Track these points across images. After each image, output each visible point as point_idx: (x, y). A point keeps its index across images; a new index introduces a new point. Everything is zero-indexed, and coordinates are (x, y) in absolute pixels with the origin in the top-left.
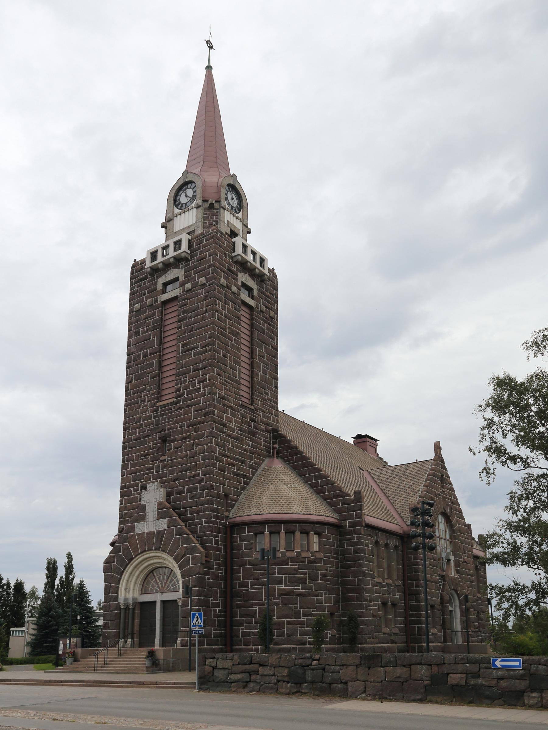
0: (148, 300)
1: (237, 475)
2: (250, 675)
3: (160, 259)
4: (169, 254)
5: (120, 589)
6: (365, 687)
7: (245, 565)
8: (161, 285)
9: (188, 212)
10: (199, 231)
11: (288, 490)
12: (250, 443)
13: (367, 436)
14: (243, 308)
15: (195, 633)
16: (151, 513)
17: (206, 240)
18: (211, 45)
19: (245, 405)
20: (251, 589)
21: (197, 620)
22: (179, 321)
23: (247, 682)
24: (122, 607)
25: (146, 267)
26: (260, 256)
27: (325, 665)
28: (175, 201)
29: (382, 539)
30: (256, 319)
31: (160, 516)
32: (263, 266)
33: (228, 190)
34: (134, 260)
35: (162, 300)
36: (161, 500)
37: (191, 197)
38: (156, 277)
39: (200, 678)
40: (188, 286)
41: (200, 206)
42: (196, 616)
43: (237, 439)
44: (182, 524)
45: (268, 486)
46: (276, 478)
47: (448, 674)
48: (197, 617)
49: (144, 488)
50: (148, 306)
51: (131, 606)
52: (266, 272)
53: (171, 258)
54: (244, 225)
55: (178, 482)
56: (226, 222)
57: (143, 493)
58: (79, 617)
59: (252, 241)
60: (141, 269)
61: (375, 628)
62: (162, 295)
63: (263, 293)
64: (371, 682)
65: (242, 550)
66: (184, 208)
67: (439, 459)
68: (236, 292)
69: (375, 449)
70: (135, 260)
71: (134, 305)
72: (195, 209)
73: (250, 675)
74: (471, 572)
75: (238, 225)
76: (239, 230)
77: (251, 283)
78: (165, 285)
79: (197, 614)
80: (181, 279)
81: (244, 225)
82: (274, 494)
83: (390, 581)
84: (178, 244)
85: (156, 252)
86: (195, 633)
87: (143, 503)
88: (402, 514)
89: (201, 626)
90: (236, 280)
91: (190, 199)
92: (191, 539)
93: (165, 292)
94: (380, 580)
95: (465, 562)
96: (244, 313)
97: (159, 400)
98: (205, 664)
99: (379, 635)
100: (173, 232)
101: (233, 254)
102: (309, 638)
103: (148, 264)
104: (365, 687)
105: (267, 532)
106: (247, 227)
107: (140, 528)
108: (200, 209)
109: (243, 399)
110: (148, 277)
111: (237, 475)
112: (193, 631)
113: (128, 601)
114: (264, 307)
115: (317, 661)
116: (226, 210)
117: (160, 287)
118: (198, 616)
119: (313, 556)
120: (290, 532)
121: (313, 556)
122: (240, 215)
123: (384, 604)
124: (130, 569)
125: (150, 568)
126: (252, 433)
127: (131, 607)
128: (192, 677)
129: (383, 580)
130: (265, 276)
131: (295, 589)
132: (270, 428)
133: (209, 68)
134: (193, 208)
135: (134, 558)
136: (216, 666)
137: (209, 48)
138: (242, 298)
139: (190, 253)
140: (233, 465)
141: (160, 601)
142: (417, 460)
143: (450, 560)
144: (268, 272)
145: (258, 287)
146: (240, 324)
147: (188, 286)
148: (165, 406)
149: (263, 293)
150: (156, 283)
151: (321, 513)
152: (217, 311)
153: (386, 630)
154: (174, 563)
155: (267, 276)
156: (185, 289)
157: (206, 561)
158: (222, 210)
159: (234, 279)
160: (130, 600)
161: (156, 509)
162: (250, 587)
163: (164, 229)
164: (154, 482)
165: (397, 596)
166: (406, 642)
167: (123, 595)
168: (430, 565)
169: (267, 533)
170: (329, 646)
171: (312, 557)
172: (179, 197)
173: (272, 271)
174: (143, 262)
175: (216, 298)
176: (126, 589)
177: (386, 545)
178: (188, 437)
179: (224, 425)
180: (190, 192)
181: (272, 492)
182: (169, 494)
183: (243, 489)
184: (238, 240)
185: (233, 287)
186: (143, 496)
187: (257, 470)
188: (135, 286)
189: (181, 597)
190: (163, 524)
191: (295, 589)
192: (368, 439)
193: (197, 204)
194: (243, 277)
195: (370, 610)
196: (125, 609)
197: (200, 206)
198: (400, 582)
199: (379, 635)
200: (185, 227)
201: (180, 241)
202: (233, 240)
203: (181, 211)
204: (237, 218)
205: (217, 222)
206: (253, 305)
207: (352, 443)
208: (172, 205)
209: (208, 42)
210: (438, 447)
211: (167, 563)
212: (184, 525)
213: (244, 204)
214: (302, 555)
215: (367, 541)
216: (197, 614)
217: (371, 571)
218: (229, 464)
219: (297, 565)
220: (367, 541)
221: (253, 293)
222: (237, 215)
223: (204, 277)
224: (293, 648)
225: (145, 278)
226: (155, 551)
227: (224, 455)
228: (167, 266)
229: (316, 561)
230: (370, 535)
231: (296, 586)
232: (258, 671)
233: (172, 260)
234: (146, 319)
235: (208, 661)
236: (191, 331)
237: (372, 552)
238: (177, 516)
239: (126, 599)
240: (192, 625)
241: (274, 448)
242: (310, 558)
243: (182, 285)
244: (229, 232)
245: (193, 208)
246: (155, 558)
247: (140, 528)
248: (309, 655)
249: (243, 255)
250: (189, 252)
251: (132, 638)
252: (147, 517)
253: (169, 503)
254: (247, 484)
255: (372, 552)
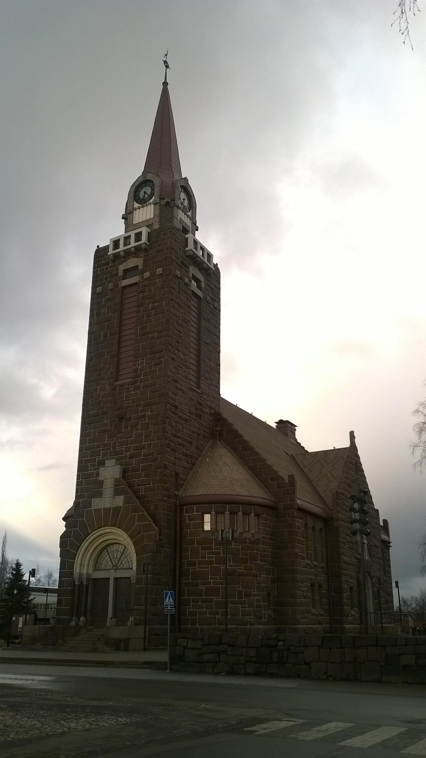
0: (110, 285)
1: (186, 455)
2: (219, 655)
3: (122, 248)
4: (130, 244)
5: (75, 565)
6: (327, 669)
7: (194, 544)
8: (122, 272)
9: (146, 207)
10: (156, 226)
11: (231, 472)
12: (197, 425)
13: (287, 422)
14: (193, 298)
15: (167, 613)
16: (108, 490)
17: (164, 235)
18: (165, 64)
19: (194, 389)
20: (199, 568)
21: (169, 599)
22: (138, 306)
23: (216, 662)
24: (77, 583)
25: (109, 254)
26: (208, 253)
27: (290, 646)
28: (135, 196)
29: (310, 522)
30: (203, 309)
31: (117, 492)
32: (210, 261)
33: (181, 191)
34: (97, 246)
35: (122, 285)
36: (118, 476)
37: (149, 194)
38: (118, 263)
39: (171, 658)
40: (147, 274)
41: (158, 203)
42: (168, 595)
43: (186, 420)
44: (137, 502)
45: (213, 468)
46: (220, 460)
47: (400, 655)
48: (169, 596)
49: (102, 463)
50: (109, 290)
51: (85, 583)
52: (212, 267)
53: (132, 247)
54: (194, 223)
55: (133, 460)
56: (179, 219)
57: (101, 469)
58: (15, 592)
59: (199, 236)
60: (104, 255)
61: (305, 609)
62: (123, 281)
63: (209, 286)
64: (333, 663)
65: (191, 529)
66: (143, 202)
67: (353, 446)
68: (188, 283)
69: (294, 434)
70: (98, 246)
71: (96, 288)
72: (153, 205)
73: (219, 655)
74: (379, 556)
75: (188, 222)
76: (189, 227)
77: (200, 276)
78: (126, 271)
79: (169, 593)
80: (140, 267)
81: (194, 223)
82: (219, 475)
83: (316, 563)
84: (138, 237)
85: (119, 240)
86: (167, 613)
87: (100, 478)
88: (325, 498)
89: (173, 605)
90: (188, 272)
91: (148, 196)
92: (146, 516)
93: (125, 278)
94: (309, 562)
95: (376, 546)
96: (193, 302)
97: (117, 380)
98: (176, 645)
99: (308, 616)
100: (133, 223)
101: (186, 248)
102: (249, 618)
103: (111, 252)
104: (327, 669)
105: (213, 512)
106: (196, 225)
107: (97, 504)
108: (158, 206)
109: (192, 383)
110: (110, 263)
111: (186, 455)
112: (166, 610)
113: (82, 578)
114: (210, 298)
115: (282, 642)
116: (179, 209)
117: (121, 273)
118: (170, 595)
119: (253, 537)
120: (233, 513)
121: (253, 537)
122: (190, 214)
123: (312, 585)
124: (85, 544)
125: (104, 544)
126: (199, 416)
127: (85, 583)
128: (163, 657)
129: (312, 562)
130: (211, 270)
131: (238, 569)
132: (213, 412)
133: (165, 84)
134: (151, 204)
135: (90, 534)
136: (187, 647)
137: (165, 67)
138: (192, 289)
139: (149, 244)
140: (183, 446)
141: (113, 579)
142: (334, 447)
143: (364, 543)
144: (214, 267)
145: (205, 280)
146: (190, 313)
147: (147, 274)
148: (123, 385)
149: (209, 286)
150: (117, 269)
151: (260, 496)
152: (172, 300)
153: (314, 611)
154: (129, 540)
155: (213, 270)
156: (144, 277)
157: (159, 539)
158: (176, 208)
159: (186, 271)
160: (85, 577)
161: (112, 486)
162: (197, 566)
163: (124, 220)
164: (111, 459)
165: (322, 578)
166: (330, 624)
167: (78, 571)
168: (349, 548)
169: (227, 513)
170: (266, 626)
171: (252, 538)
172: (138, 193)
173: (216, 266)
174: (107, 247)
175: (172, 288)
176: (81, 565)
177: (314, 527)
178: (144, 416)
179: (176, 407)
180: (149, 190)
181: (217, 473)
182: (125, 472)
183: (191, 469)
184: (189, 236)
185: (185, 279)
186: (100, 472)
187: (202, 451)
188: (98, 270)
189: (135, 574)
190: (120, 501)
191: (238, 569)
192: (289, 425)
193: (155, 201)
194: (193, 270)
195: (302, 591)
196: (79, 585)
197: (158, 203)
198: (324, 565)
199: (308, 616)
200: (144, 220)
201: (140, 233)
202: (187, 236)
203: (140, 205)
204: (188, 216)
205: (172, 218)
206: (201, 296)
207: (275, 427)
208: (133, 199)
209: (165, 62)
210: (352, 435)
211: (120, 538)
212: (139, 502)
213: (194, 204)
214: (245, 535)
215: (299, 523)
216: (169, 593)
217: (302, 553)
218: (180, 445)
219: (239, 545)
220: (299, 523)
221: (201, 285)
222: (188, 213)
223: (161, 268)
224: (236, 628)
225: (107, 264)
226: (110, 527)
227: (175, 436)
228: (128, 254)
229: (256, 542)
230: (301, 518)
231: (239, 566)
232: (227, 652)
233: (133, 250)
234: (107, 301)
235: (179, 641)
236: (149, 316)
237: (303, 535)
238: (133, 493)
239: (80, 575)
240: (165, 604)
241: (216, 431)
242: (251, 538)
243: (142, 273)
244: (181, 228)
245: (151, 204)
246: (110, 534)
247: (97, 504)
248: (275, 636)
249: (194, 250)
250: (148, 243)
251: (85, 616)
252: (104, 493)
253: (125, 480)
254: (193, 464)
255: (303, 535)
